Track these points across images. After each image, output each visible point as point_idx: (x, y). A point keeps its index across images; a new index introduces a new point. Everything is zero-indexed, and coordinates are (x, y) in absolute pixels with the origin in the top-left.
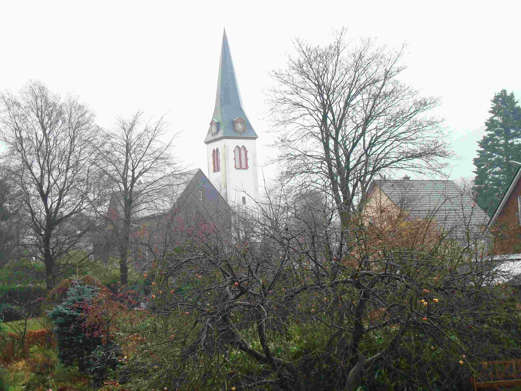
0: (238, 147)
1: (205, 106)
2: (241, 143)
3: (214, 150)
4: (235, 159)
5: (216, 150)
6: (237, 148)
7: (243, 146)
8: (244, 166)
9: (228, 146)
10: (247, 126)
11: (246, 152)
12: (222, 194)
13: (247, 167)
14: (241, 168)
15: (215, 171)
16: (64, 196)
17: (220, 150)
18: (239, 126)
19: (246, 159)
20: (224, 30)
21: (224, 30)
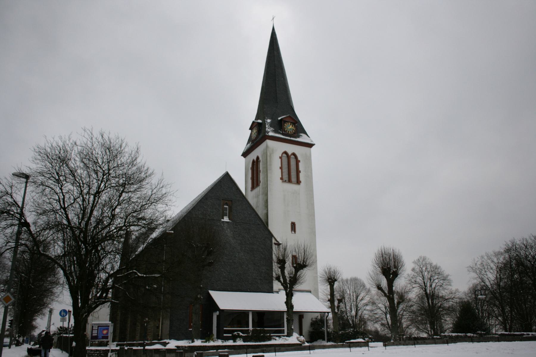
0: (285, 153)
1: (248, 104)
2: (291, 149)
3: (253, 161)
4: (281, 168)
5: (255, 159)
6: (284, 155)
7: (294, 154)
8: (294, 179)
9: (275, 149)
10: (299, 129)
11: (298, 162)
12: (260, 212)
13: (298, 182)
14: (290, 181)
15: (253, 188)
16: (398, 307)
17: (260, 158)
18: (290, 127)
19: (298, 172)
20: (273, 29)
21: (273, 29)
